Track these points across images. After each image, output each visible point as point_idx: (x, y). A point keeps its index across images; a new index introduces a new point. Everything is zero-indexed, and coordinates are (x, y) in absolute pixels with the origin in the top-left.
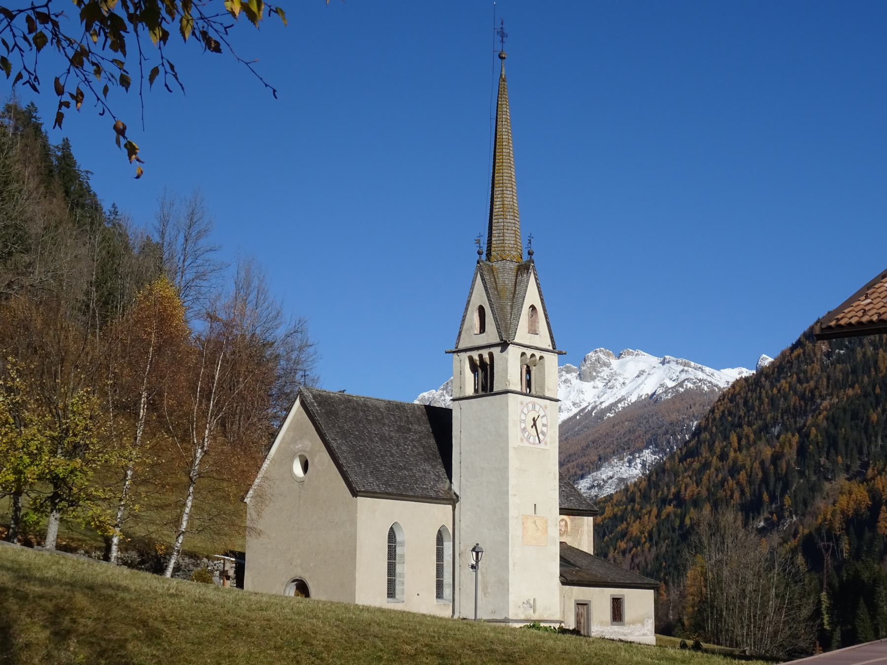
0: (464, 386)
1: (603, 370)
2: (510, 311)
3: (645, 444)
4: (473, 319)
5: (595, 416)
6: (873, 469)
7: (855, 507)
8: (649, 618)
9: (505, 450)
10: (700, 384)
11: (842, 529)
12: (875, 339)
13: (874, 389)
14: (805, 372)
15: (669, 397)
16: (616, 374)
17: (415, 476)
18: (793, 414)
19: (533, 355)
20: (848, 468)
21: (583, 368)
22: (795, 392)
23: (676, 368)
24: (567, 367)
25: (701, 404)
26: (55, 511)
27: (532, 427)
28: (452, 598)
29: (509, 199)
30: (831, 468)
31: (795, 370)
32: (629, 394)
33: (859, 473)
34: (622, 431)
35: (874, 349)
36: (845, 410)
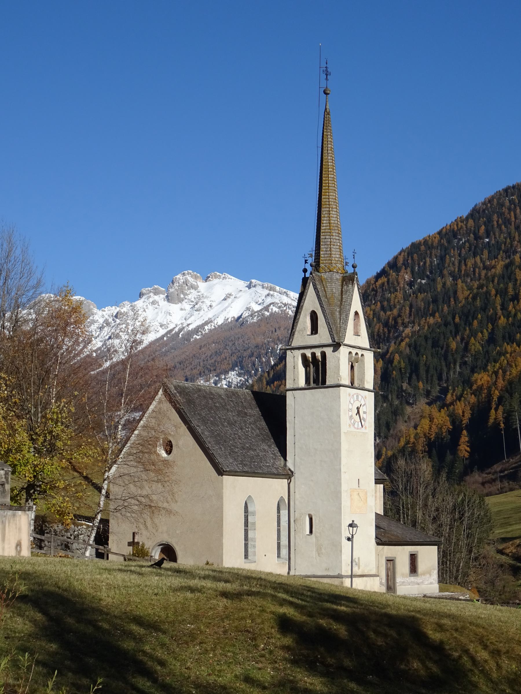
0: (298, 379)
1: (191, 293)
2: (338, 316)
3: (231, 366)
4: (306, 322)
5: (182, 338)
6: (452, 395)
7: (437, 431)
8: (434, 569)
9: (337, 435)
10: (285, 308)
11: (425, 451)
12: (454, 270)
13: (454, 318)
14: (389, 300)
15: (255, 321)
16: (203, 297)
17: (259, 455)
18: (377, 340)
19: (357, 354)
20: (428, 394)
21: (171, 290)
22: (379, 320)
23: (262, 292)
24: (155, 289)
25: (285, 328)
26: (30, 500)
27: (356, 415)
28: (288, 557)
29: (334, 219)
30: (413, 393)
31: (379, 298)
32: (216, 316)
33: (438, 398)
34: (209, 353)
35: (453, 280)
36: (426, 338)
